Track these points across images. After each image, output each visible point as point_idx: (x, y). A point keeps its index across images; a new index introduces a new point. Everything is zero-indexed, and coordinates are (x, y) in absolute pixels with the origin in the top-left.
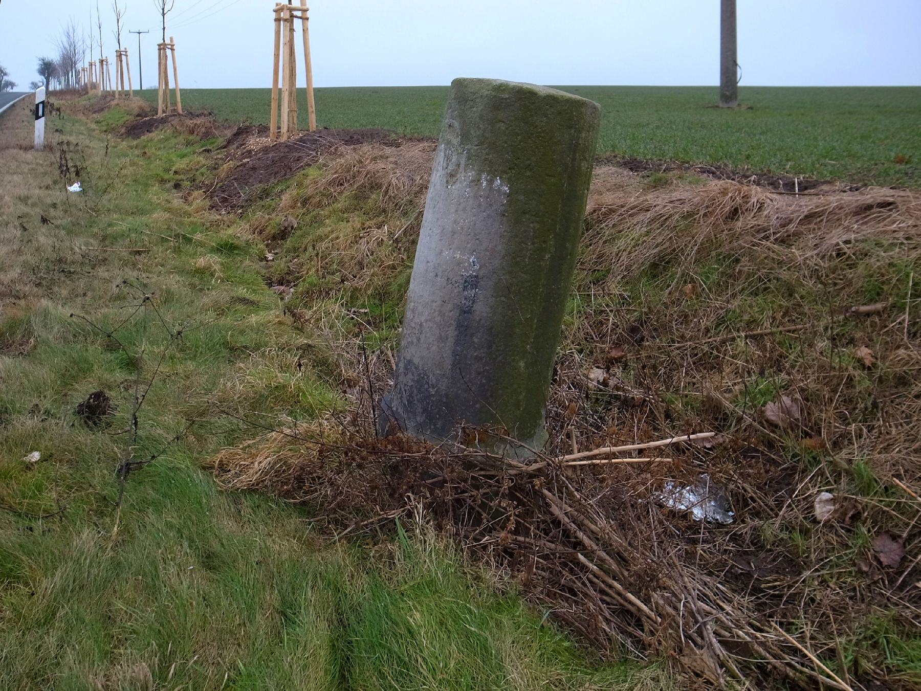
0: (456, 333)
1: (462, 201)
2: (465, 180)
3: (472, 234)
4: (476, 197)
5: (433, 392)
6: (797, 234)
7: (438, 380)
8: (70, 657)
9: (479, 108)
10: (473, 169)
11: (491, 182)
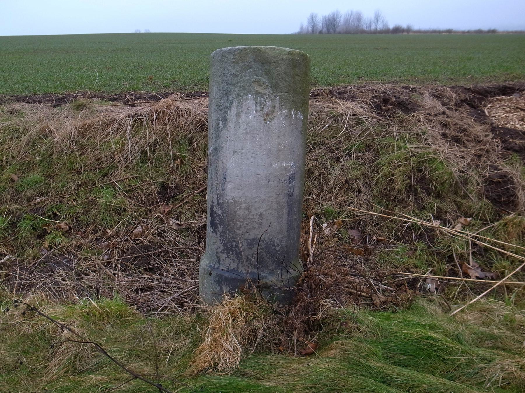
0: (288, 210)
1: (282, 130)
2: (281, 116)
3: (291, 149)
4: (290, 125)
5: (278, 248)
6: (392, 82)
7: (281, 241)
8: (503, 57)
9: (282, 67)
10: (286, 108)
11: (296, 114)
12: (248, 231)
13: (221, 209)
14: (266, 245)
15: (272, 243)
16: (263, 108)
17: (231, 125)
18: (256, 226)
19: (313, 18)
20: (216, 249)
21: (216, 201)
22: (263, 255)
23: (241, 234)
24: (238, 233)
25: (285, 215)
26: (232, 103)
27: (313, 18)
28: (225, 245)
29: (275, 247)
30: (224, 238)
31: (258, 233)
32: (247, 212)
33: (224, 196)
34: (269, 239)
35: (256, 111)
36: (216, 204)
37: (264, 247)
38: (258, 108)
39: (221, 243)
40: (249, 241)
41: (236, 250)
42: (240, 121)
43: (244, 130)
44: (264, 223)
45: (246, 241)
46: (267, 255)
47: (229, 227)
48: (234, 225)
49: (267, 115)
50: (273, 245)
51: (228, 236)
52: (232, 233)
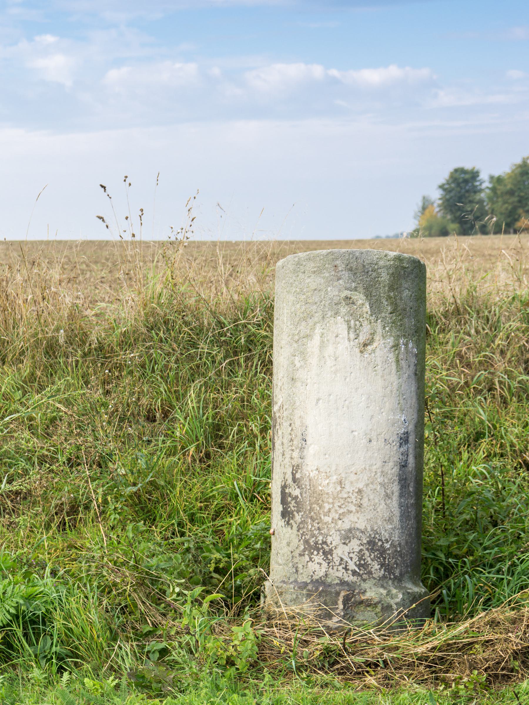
10: (391, 335)
11: (406, 345)
12: (341, 517)
13: (299, 487)
14: (368, 539)
15: (377, 536)
16: (358, 335)
17: (314, 361)
18: (353, 508)
19: (474, 168)
20: (292, 552)
21: (291, 476)
22: (364, 554)
23: (330, 522)
24: (325, 521)
25: (396, 494)
26: (313, 329)
27: (474, 168)
28: (307, 542)
29: (383, 543)
30: (304, 532)
31: (357, 520)
32: (339, 488)
33: (304, 467)
34: (372, 530)
35: (349, 339)
36: (290, 481)
37: (365, 542)
38: (352, 336)
39: (300, 541)
40: (343, 532)
41: (323, 548)
42: (326, 355)
43: (331, 367)
44: (365, 505)
45: (338, 533)
46: (370, 555)
47: (312, 514)
48: (320, 508)
49: (365, 345)
50: (379, 540)
51: (310, 527)
52: (317, 521)
